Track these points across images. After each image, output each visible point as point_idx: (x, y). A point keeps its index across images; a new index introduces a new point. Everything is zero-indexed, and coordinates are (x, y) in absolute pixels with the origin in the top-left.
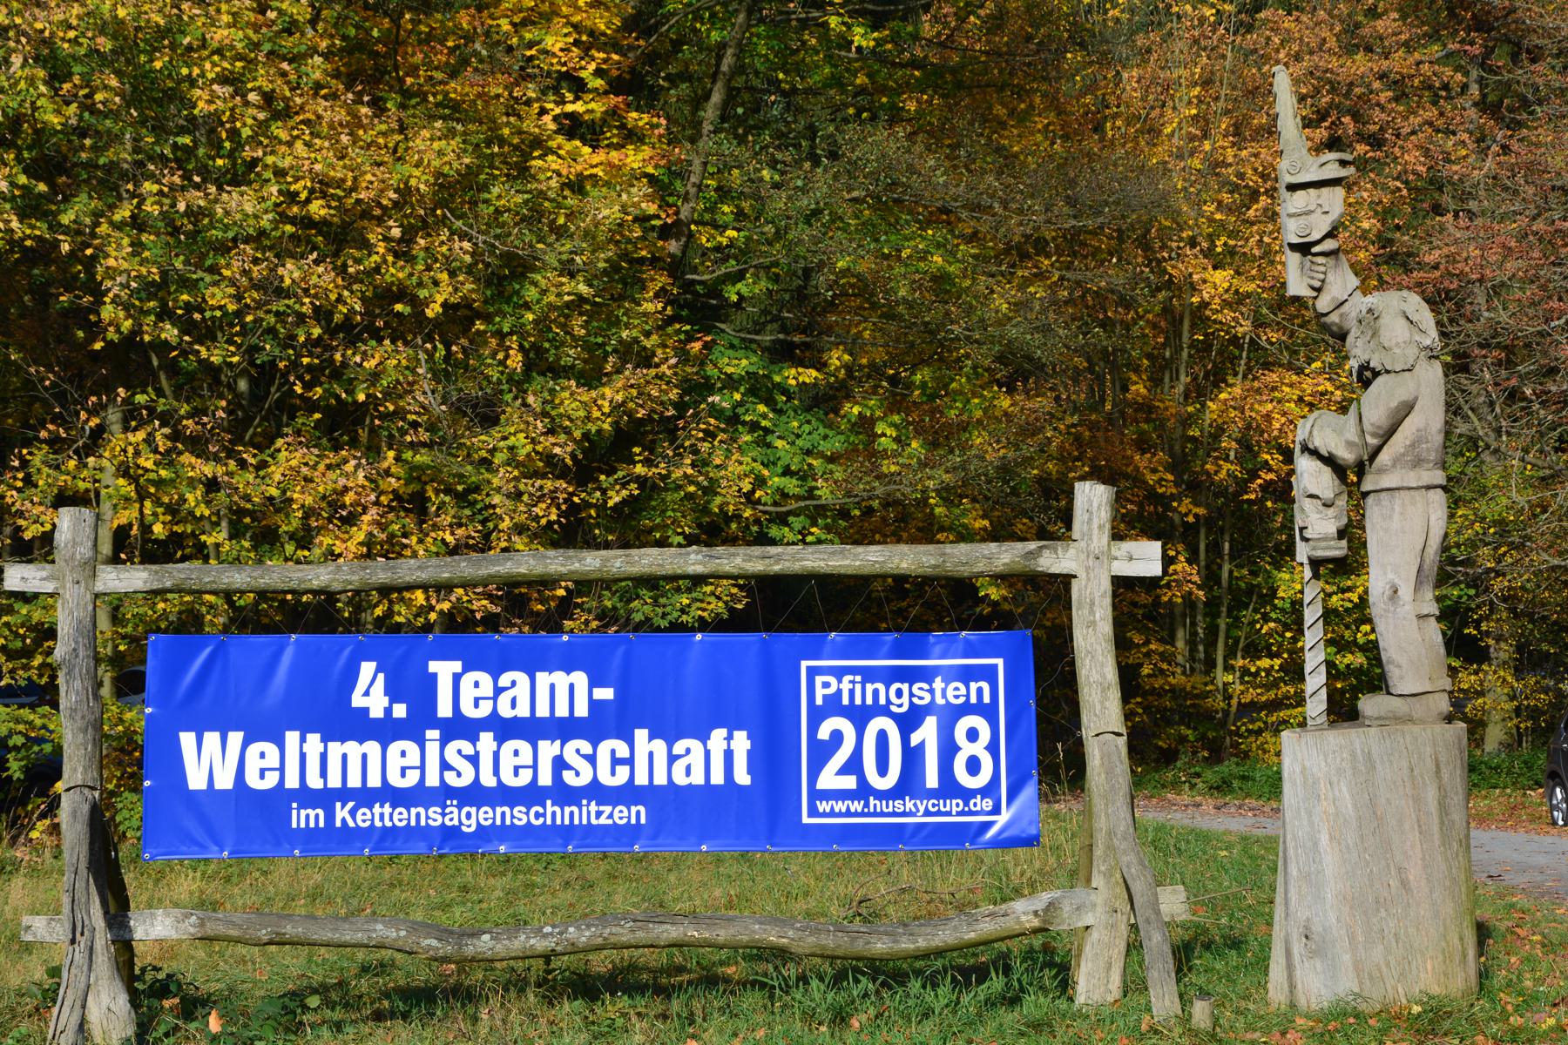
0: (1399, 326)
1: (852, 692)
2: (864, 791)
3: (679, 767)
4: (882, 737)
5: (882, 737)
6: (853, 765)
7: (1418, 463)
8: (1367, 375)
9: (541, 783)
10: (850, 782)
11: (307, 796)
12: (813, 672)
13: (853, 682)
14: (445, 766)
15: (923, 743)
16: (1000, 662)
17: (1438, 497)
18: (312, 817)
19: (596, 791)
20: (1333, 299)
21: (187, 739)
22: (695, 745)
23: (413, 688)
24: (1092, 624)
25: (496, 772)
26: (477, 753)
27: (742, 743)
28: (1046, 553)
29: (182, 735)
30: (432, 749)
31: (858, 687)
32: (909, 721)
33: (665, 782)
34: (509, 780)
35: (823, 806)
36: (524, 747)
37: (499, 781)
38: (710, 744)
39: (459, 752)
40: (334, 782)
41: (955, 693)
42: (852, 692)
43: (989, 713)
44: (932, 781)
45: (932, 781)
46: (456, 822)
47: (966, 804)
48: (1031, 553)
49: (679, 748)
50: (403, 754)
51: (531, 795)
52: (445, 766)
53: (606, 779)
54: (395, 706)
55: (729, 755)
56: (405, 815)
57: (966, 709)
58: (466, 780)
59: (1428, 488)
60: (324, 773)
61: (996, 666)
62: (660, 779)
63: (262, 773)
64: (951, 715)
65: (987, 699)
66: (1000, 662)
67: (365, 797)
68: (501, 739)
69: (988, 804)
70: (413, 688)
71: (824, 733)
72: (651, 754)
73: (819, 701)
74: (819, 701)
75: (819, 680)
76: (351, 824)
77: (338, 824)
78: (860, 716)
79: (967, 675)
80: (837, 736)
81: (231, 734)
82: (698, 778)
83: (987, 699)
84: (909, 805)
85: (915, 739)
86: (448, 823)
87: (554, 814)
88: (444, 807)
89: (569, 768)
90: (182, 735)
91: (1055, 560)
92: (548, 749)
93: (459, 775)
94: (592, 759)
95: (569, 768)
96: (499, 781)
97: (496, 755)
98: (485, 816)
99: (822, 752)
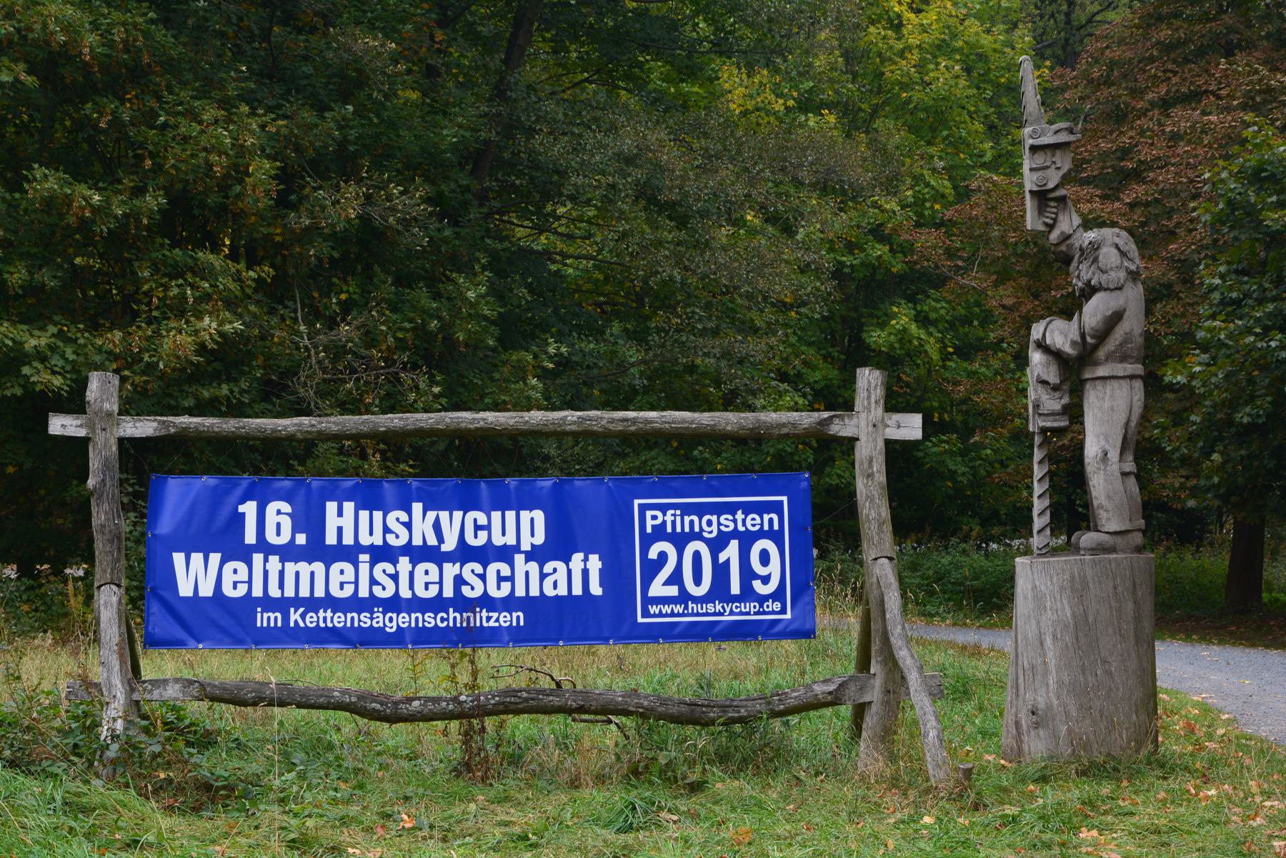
0: (1109, 250)
1: (674, 523)
2: (684, 597)
3: (548, 582)
4: (697, 556)
5: (697, 556)
6: (676, 578)
7: (1124, 359)
8: (1090, 290)
9: (445, 595)
10: (673, 591)
11: (268, 603)
12: (643, 508)
13: (674, 515)
14: (373, 582)
15: (728, 560)
16: (785, 499)
17: (1138, 385)
18: (274, 618)
19: (486, 601)
20: (1062, 233)
21: (178, 558)
22: (560, 565)
23: (310, 520)
24: (870, 476)
25: (411, 587)
26: (397, 573)
27: (595, 563)
28: (836, 421)
29: (175, 555)
30: (364, 568)
31: (678, 519)
32: (717, 545)
33: (537, 594)
34: (421, 592)
35: (654, 609)
36: (432, 568)
37: (414, 593)
38: (571, 565)
39: (384, 571)
40: (289, 592)
41: (753, 522)
42: (674, 523)
43: (776, 537)
44: (735, 589)
45: (735, 589)
46: (381, 625)
47: (761, 606)
48: (825, 420)
49: (548, 568)
50: (235, 571)
51: (437, 604)
52: (373, 582)
53: (493, 592)
54: (298, 536)
55: (585, 573)
56: (758, 521)
57: (761, 534)
58: (389, 593)
59: (1132, 377)
60: (281, 586)
61: (782, 502)
62: (534, 592)
63: (427, 586)
64: (747, 540)
65: (776, 527)
66: (785, 499)
67: (312, 604)
68: (414, 563)
69: (777, 606)
70: (310, 520)
71: (653, 554)
72: (527, 573)
73: (649, 530)
74: (649, 530)
75: (649, 514)
76: (302, 625)
77: (292, 625)
78: (680, 541)
79: (761, 509)
80: (663, 556)
81: (211, 555)
82: (562, 591)
83: (776, 527)
84: (719, 607)
85: (722, 557)
86: (375, 625)
87: (455, 618)
88: (372, 613)
89: (467, 584)
90: (175, 555)
91: (843, 428)
92: (451, 570)
93: (473, 588)
94: (483, 577)
95: (467, 583)
96: (414, 593)
97: (411, 574)
98: (404, 620)
99: (652, 568)
